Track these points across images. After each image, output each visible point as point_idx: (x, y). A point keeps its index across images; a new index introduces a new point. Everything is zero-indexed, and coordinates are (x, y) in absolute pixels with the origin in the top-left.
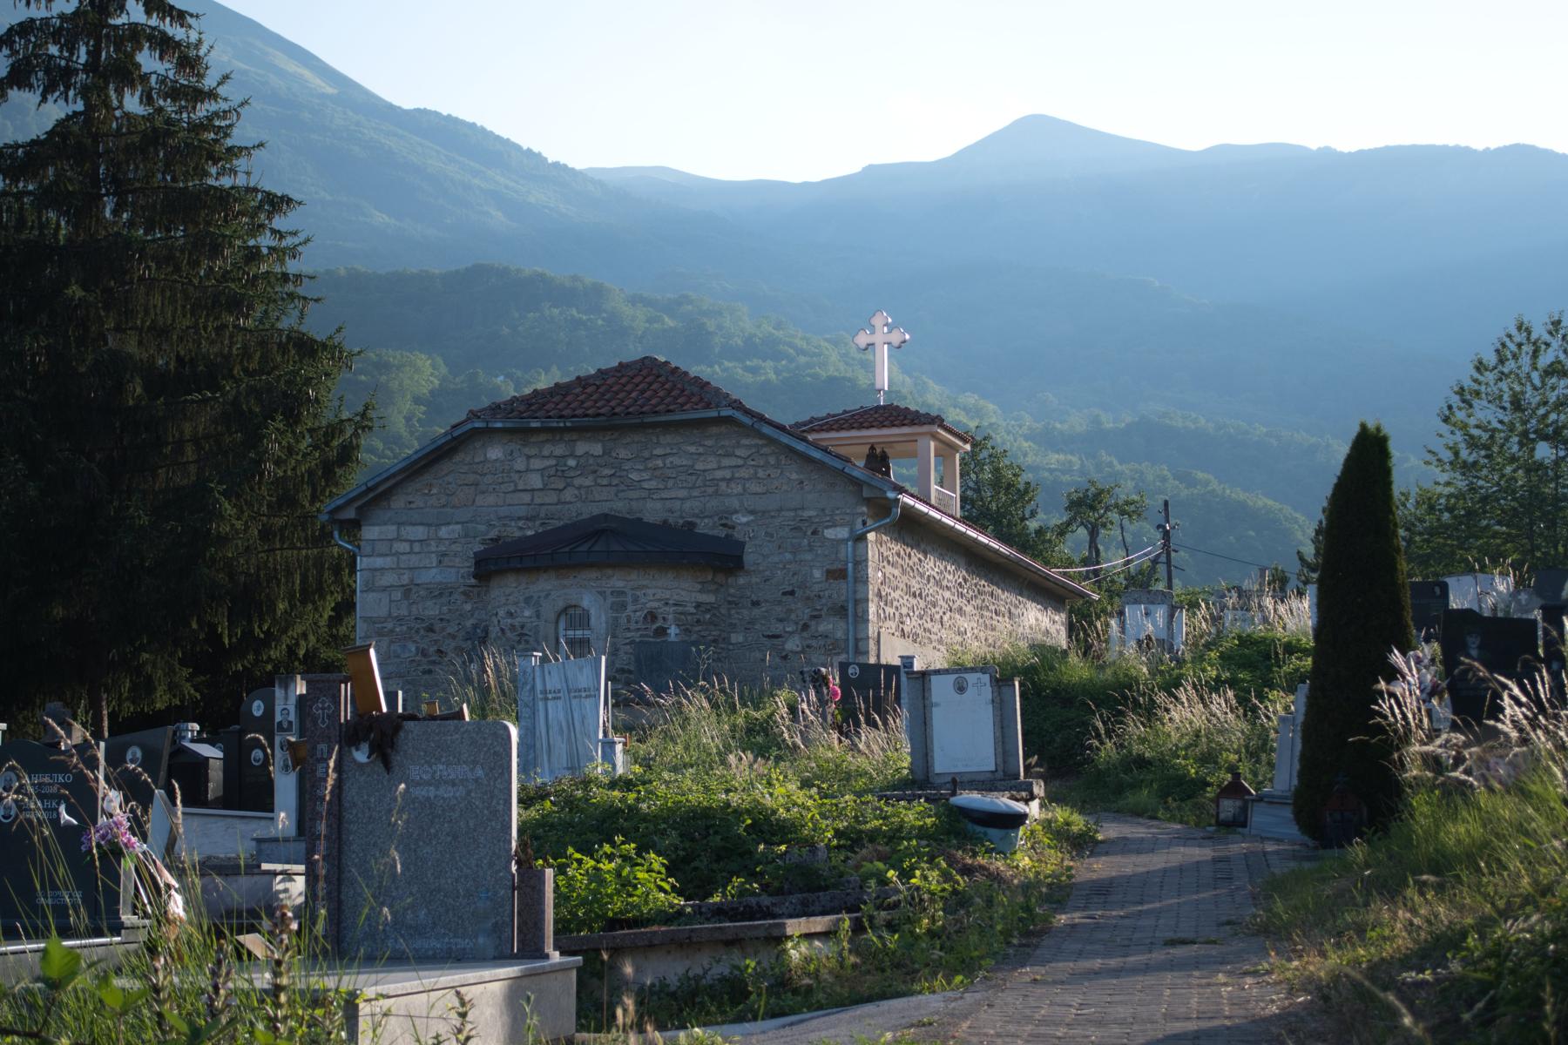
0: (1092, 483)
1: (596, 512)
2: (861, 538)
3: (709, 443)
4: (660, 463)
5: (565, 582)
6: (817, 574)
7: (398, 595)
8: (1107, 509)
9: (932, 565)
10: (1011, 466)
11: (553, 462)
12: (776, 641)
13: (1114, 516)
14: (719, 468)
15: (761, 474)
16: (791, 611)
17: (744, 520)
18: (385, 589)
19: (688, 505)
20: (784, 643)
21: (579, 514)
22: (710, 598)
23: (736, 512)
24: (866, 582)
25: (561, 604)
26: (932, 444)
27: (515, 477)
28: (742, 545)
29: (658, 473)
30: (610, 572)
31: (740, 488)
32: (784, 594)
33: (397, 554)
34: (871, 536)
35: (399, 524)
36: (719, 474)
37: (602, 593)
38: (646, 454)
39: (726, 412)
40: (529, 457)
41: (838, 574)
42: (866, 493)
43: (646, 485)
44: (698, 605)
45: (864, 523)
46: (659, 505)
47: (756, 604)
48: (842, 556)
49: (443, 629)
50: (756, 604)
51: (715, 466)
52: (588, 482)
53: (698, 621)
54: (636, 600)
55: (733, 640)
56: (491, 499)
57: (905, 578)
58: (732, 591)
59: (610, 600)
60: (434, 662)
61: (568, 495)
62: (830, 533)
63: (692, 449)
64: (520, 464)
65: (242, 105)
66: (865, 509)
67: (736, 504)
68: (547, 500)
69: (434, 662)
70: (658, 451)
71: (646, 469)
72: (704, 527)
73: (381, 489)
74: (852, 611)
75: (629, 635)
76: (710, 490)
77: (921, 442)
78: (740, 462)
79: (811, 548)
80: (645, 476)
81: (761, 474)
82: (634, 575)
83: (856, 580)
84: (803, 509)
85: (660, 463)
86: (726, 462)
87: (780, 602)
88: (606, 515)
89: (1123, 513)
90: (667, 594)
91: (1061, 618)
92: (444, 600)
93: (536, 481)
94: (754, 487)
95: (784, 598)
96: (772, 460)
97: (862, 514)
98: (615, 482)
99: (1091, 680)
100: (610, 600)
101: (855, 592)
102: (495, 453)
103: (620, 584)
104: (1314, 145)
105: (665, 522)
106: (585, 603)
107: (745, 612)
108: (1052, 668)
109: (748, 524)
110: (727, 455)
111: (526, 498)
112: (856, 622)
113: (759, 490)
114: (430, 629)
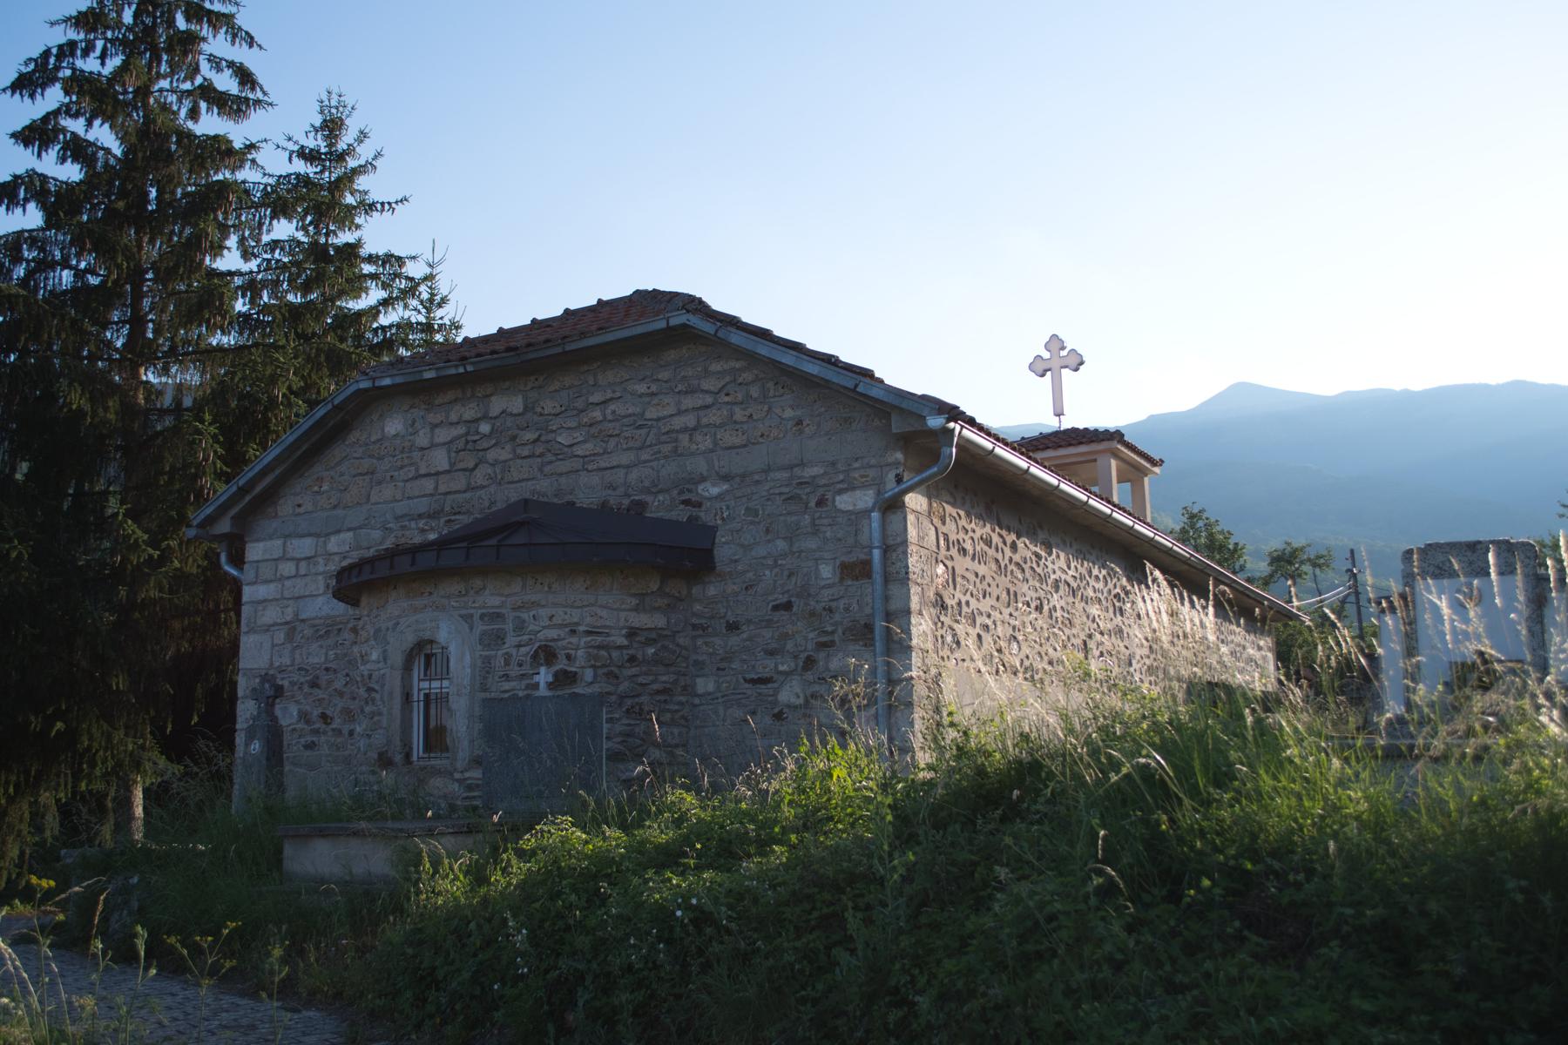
0: (1288, 544)
1: (514, 497)
2: (894, 506)
3: (664, 375)
4: (597, 414)
5: (419, 602)
6: (826, 571)
7: (280, 637)
8: (1302, 563)
9: (1060, 564)
10: (1222, 532)
11: (461, 430)
12: (763, 689)
13: (1306, 568)
14: (680, 413)
15: (739, 414)
16: (785, 637)
17: (715, 491)
18: (267, 629)
19: (634, 475)
20: (776, 691)
21: (493, 503)
22: (659, 621)
23: (703, 479)
24: (904, 579)
25: (410, 639)
26: (1113, 463)
27: (416, 455)
28: (713, 530)
29: (593, 430)
30: (478, 583)
31: (708, 443)
32: (776, 608)
33: (282, 579)
34: (915, 501)
35: (287, 536)
36: (678, 422)
37: (467, 618)
38: (580, 404)
39: (678, 319)
40: (434, 426)
41: (857, 570)
42: (897, 426)
43: (579, 451)
44: (632, 633)
45: (899, 480)
46: (595, 479)
47: (733, 627)
48: (864, 539)
49: (330, 682)
50: (733, 627)
51: (671, 410)
52: (504, 454)
53: (632, 659)
54: (520, 627)
55: (700, 689)
56: (388, 492)
57: (1004, 581)
58: (698, 607)
59: (480, 627)
60: (316, 732)
61: (479, 477)
62: (844, 502)
63: (641, 388)
64: (422, 439)
65: (375, 158)
66: (899, 456)
67: (701, 466)
68: (455, 486)
69: (316, 732)
70: (596, 397)
71: (580, 426)
72: (660, 507)
73: (258, 489)
74: (883, 634)
75: (507, 686)
76: (666, 448)
77: (1101, 460)
78: (709, 400)
79: (815, 530)
80: (579, 436)
81: (739, 414)
82: (516, 586)
83: (887, 579)
84: (802, 464)
85: (597, 414)
86: (688, 402)
87: (769, 623)
88: (526, 501)
89: (1315, 565)
90: (575, 616)
91: (1266, 642)
92: (330, 642)
93: (440, 459)
94: (730, 438)
95: (777, 615)
96: (755, 391)
97: (897, 464)
98: (539, 451)
99: (1376, 824)
100: (480, 627)
101: (887, 599)
102: (394, 425)
103: (495, 601)
104: (1398, 388)
105: (604, 504)
106: (442, 636)
107: (718, 641)
108: (1223, 777)
109: (720, 497)
110: (691, 391)
111: (428, 485)
112: (888, 652)
113: (737, 441)
114: (314, 684)
